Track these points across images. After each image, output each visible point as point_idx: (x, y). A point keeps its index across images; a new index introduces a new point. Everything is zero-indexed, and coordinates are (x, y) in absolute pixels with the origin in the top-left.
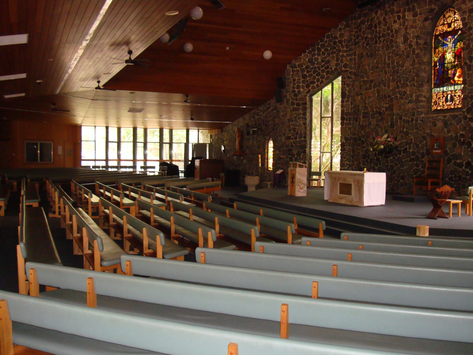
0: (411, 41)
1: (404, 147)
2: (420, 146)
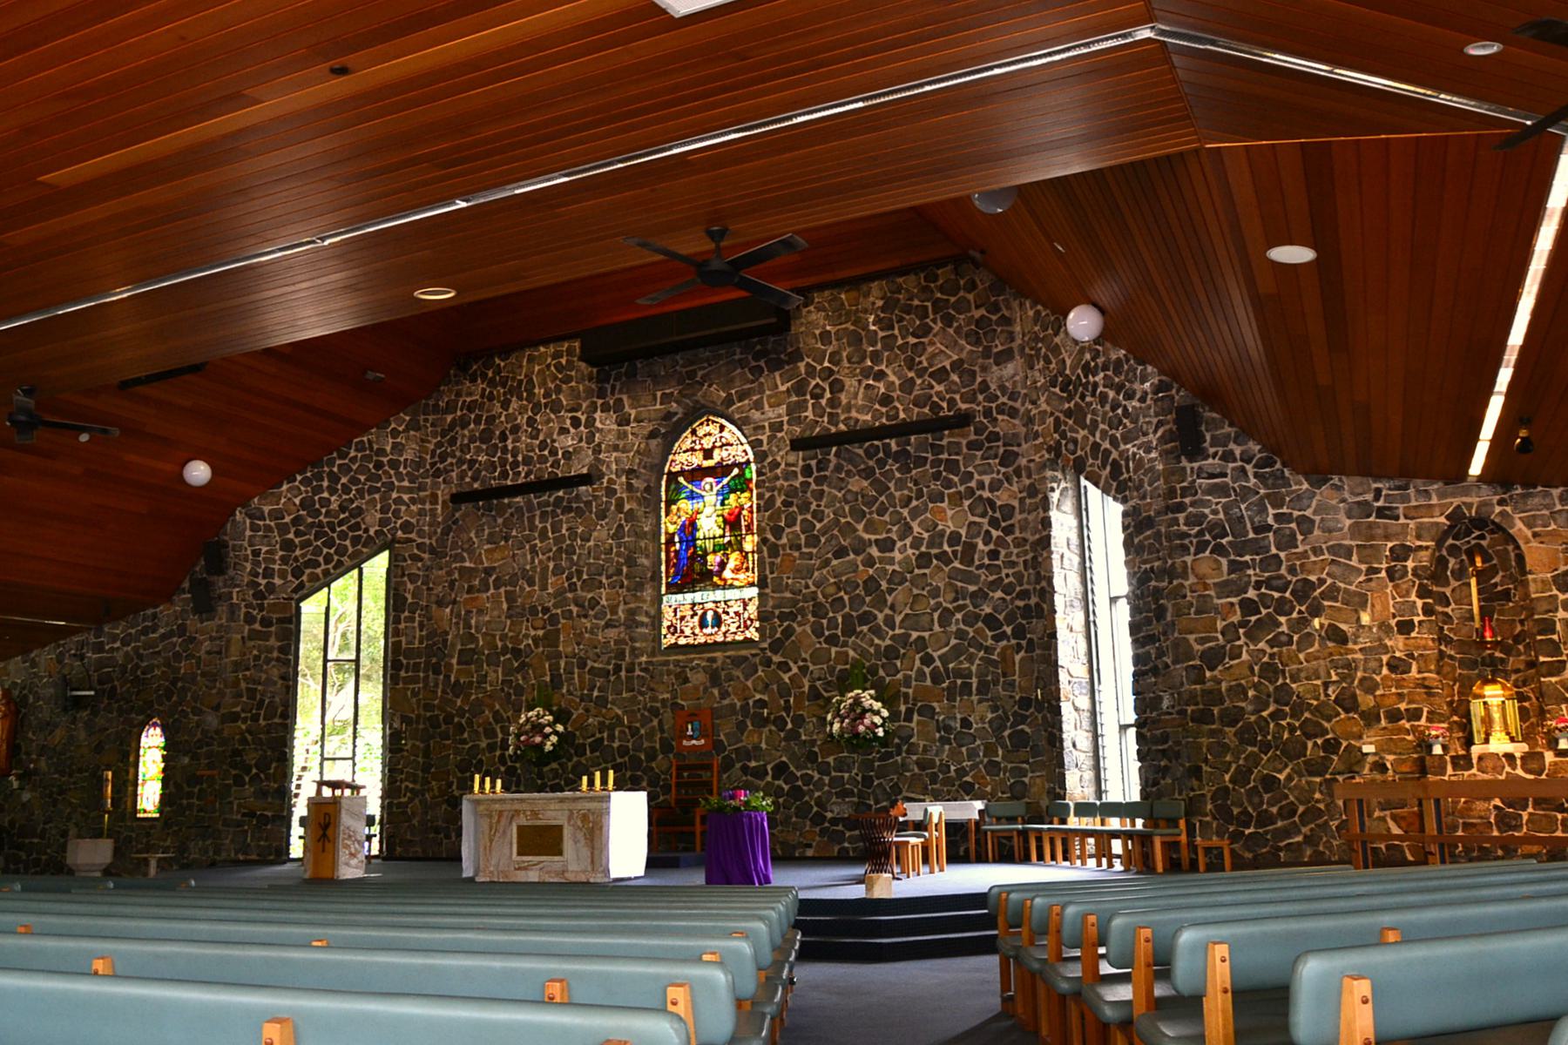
0: (610, 481)
1: (593, 735)
2: (643, 731)
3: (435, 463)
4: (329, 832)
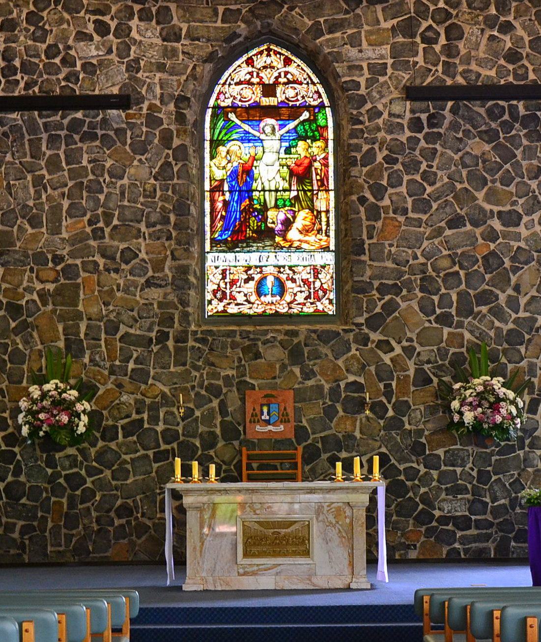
1: (128, 416)
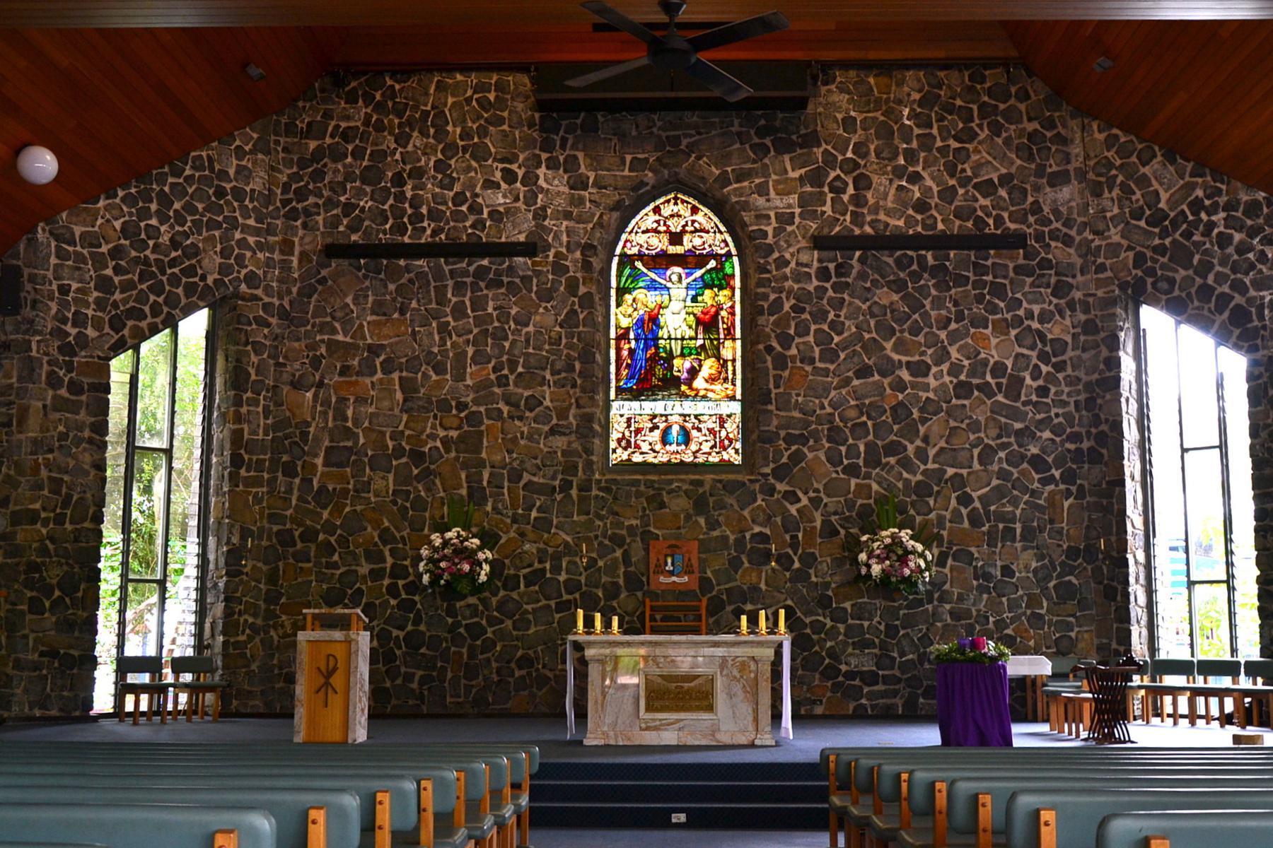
1: (530, 565)
2: (601, 563)
3: (289, 201)
4: (337, 680)
